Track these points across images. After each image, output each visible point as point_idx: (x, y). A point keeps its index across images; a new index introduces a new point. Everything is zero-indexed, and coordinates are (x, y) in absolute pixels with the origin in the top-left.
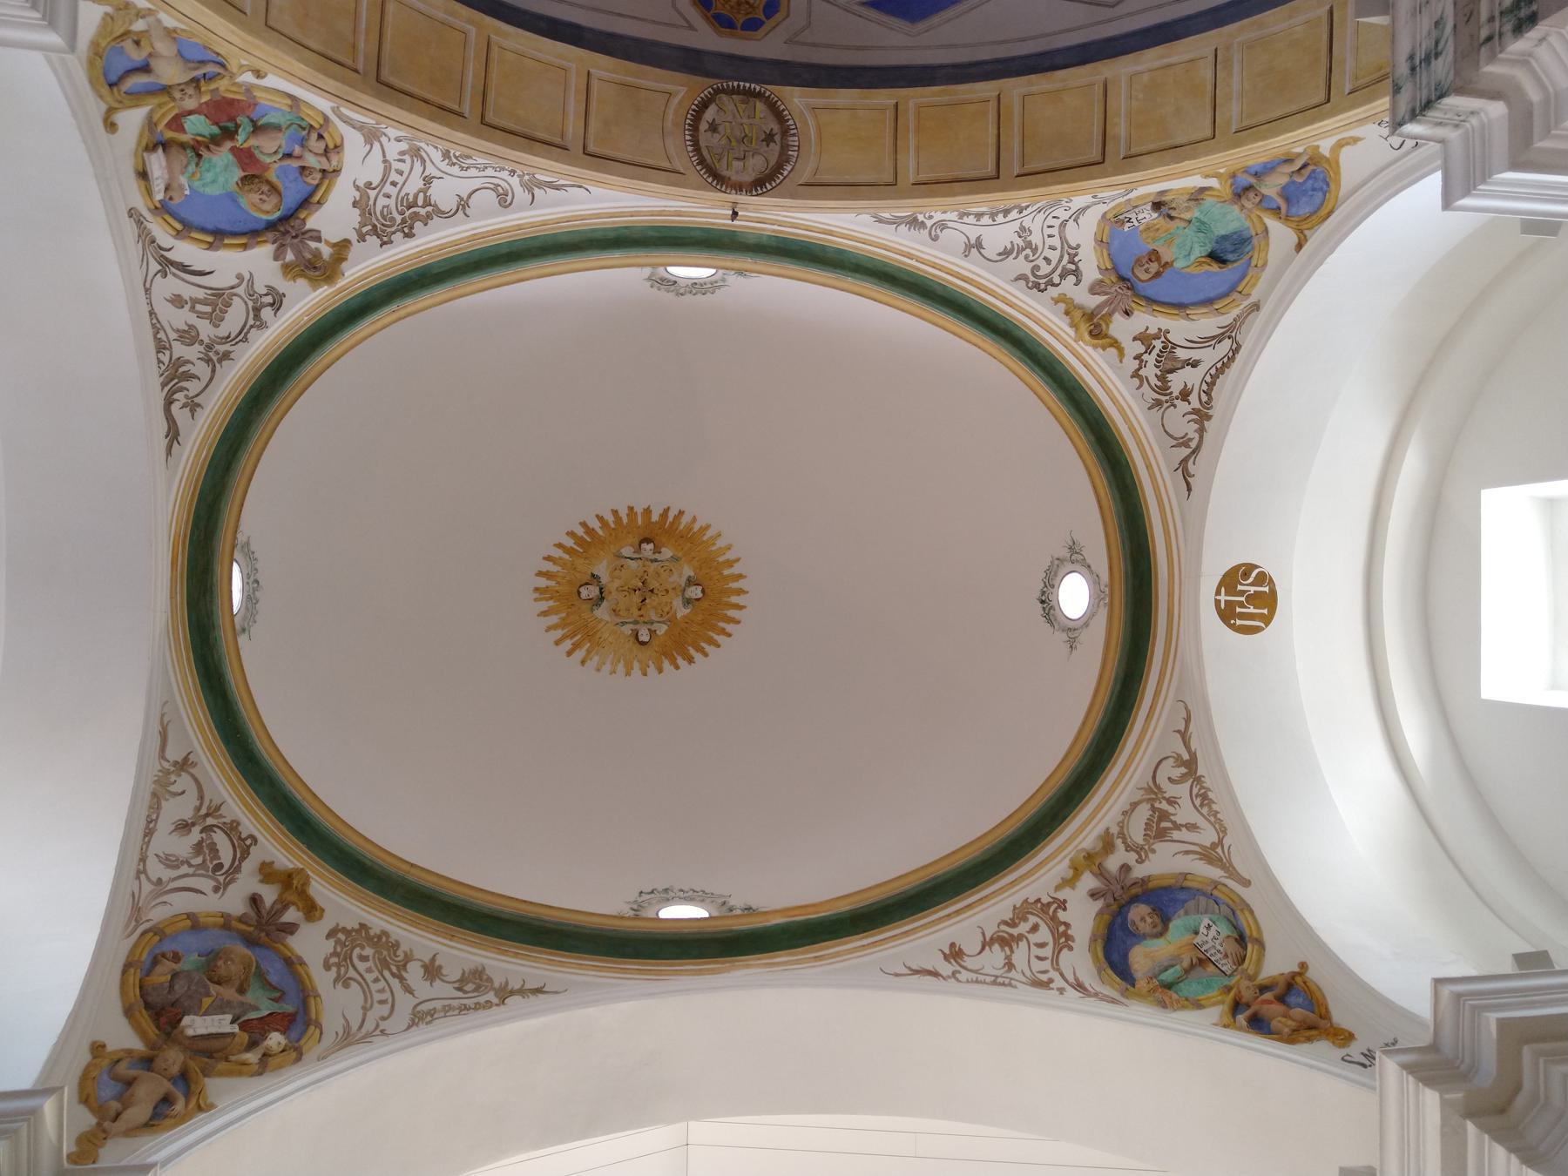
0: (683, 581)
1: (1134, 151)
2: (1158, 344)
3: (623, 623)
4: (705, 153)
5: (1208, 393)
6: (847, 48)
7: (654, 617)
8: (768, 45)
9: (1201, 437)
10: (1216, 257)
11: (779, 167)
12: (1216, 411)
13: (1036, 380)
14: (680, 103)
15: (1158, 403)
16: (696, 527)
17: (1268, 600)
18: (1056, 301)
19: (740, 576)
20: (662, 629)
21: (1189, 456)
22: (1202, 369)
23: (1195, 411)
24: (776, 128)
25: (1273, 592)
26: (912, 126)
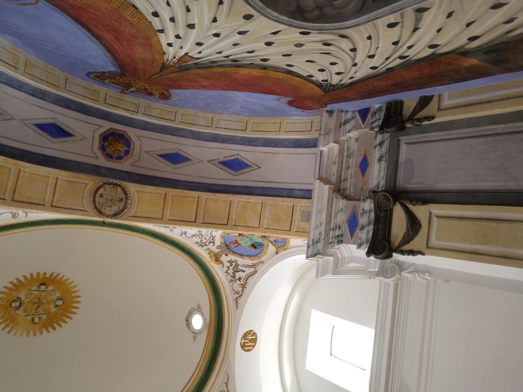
0: (55, 298)
1: (237, 224)
2: (234, 264)
3: (28, 315)
4: (97, 204)
5: (246, 280)
6: (151, 169)
7: (41, 312)
8: (124, 166)
9: (242, 293)
10: (254, 246)
11: (123, 210)
12: (248, 286)
13: (196, 266)
14: (90, 187)
15: (232, 281)
16: (64, 279)
17: (254, 341)
18: (206, 250)
19: (79, 297)
20: (44, 317)
21: (239, 296)
22: (245, 273)
23: (242, 284)
24: (124, 196)
25: (256, 338)
26: (170, 201)
